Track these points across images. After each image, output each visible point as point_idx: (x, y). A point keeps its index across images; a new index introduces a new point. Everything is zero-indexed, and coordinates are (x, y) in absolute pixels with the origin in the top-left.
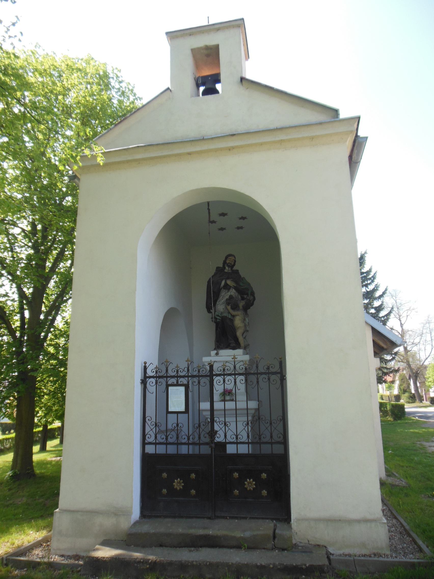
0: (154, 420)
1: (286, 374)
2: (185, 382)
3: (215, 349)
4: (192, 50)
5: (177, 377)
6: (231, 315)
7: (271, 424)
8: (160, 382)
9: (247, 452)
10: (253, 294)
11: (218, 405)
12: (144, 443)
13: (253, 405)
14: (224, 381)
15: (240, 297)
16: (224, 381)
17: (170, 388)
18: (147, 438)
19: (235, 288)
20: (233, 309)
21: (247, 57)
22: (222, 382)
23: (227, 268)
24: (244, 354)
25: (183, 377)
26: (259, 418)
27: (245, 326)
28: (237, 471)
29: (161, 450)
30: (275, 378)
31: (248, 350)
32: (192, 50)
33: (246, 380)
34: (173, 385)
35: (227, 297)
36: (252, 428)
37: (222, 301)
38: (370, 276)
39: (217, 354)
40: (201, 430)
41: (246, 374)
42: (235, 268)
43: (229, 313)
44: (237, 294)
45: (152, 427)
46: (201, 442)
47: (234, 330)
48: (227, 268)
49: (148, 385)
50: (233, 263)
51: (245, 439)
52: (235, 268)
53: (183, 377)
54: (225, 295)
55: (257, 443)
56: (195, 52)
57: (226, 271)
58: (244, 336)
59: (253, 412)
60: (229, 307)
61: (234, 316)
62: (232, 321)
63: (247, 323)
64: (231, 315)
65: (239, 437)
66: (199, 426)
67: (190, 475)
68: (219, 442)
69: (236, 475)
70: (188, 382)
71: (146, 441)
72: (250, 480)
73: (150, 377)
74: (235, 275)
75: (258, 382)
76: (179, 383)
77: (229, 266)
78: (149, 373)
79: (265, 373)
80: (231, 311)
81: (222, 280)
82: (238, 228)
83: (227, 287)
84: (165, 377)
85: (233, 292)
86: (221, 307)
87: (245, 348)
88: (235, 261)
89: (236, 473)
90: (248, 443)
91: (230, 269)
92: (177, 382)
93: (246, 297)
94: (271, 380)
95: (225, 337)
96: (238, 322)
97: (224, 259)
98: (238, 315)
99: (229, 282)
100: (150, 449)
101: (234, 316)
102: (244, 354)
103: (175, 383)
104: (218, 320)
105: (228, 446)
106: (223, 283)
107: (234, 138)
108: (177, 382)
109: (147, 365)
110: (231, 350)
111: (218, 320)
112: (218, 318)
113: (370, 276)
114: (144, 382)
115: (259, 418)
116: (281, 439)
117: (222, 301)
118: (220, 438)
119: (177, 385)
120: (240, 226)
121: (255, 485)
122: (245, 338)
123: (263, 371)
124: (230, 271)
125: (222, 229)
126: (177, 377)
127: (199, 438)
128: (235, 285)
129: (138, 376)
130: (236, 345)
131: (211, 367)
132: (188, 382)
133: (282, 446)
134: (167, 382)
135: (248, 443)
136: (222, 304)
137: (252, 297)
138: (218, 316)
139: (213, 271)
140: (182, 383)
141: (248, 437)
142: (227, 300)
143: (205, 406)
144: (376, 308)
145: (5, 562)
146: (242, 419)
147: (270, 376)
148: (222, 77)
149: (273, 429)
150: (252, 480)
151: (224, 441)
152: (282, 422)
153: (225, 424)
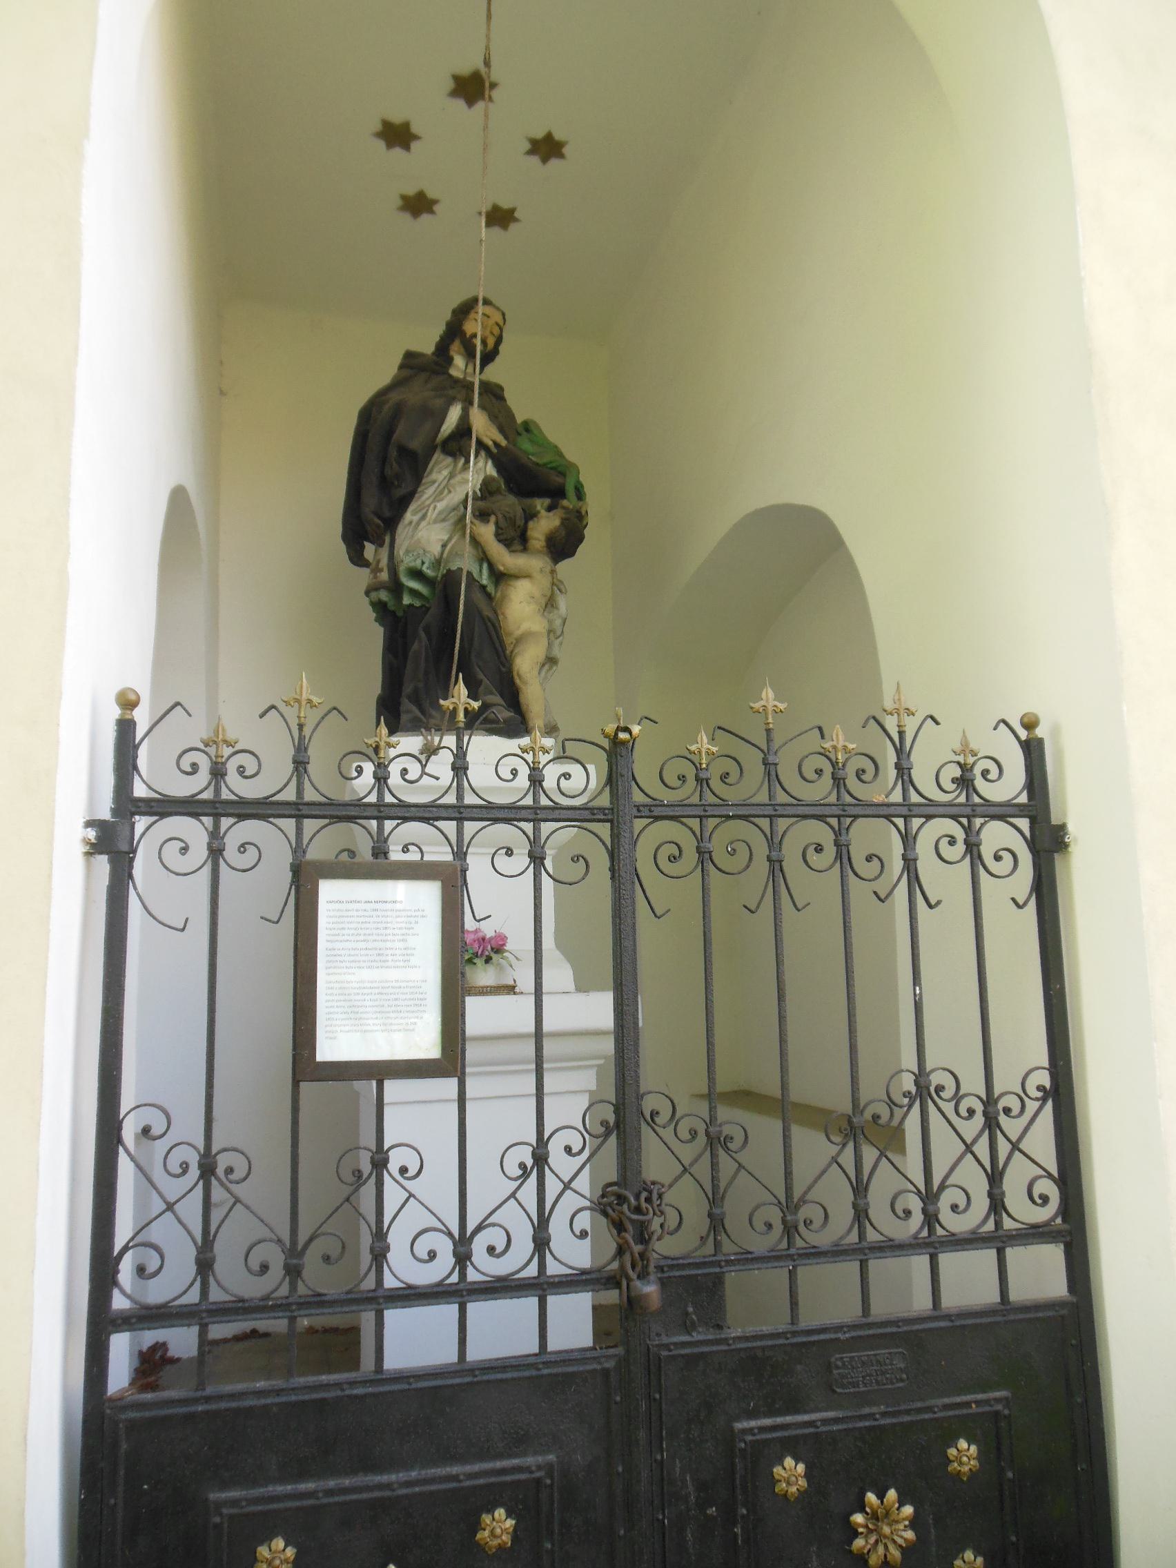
0: (190, 1127)
2: (440, 853)
7: (991, 1124)
8: (243, 848)
12: (101, 1323)
25: (428, 814)
28: (792, 1446)
34: (348, 868)
37: (440, 506)
40: (553, 1187)
43: (484, 557)
45: (173, 1188)
46: (553, 1268)
53: (428, 814)
60: (487, 532)
61: (499, 577)
66: (540, 1159)
67: (476, 1526)
69: (791, 1473)
71: (119, 1302)
72: (881, 1496)
73: (162, 807)
75: (910, 863)
80: (497, 551)
86: (430, 531)
89: (789, 1462)
96: (521, 608)
98: (528, 576)
104: (407, 600)
108: (380, 851)
111: (407, 600)
114: (111, 842)
119: (379, 866)
121: (914, 1523)
127: (541, 1243)
129: (77, 790)
132: (460, 854)
133: (1052, 1256)
134: (298, 849)
136: (435, 522)
139: (385, 372)
140: (413, 856)
149: (1003, 1148)
150: (892, 1494)
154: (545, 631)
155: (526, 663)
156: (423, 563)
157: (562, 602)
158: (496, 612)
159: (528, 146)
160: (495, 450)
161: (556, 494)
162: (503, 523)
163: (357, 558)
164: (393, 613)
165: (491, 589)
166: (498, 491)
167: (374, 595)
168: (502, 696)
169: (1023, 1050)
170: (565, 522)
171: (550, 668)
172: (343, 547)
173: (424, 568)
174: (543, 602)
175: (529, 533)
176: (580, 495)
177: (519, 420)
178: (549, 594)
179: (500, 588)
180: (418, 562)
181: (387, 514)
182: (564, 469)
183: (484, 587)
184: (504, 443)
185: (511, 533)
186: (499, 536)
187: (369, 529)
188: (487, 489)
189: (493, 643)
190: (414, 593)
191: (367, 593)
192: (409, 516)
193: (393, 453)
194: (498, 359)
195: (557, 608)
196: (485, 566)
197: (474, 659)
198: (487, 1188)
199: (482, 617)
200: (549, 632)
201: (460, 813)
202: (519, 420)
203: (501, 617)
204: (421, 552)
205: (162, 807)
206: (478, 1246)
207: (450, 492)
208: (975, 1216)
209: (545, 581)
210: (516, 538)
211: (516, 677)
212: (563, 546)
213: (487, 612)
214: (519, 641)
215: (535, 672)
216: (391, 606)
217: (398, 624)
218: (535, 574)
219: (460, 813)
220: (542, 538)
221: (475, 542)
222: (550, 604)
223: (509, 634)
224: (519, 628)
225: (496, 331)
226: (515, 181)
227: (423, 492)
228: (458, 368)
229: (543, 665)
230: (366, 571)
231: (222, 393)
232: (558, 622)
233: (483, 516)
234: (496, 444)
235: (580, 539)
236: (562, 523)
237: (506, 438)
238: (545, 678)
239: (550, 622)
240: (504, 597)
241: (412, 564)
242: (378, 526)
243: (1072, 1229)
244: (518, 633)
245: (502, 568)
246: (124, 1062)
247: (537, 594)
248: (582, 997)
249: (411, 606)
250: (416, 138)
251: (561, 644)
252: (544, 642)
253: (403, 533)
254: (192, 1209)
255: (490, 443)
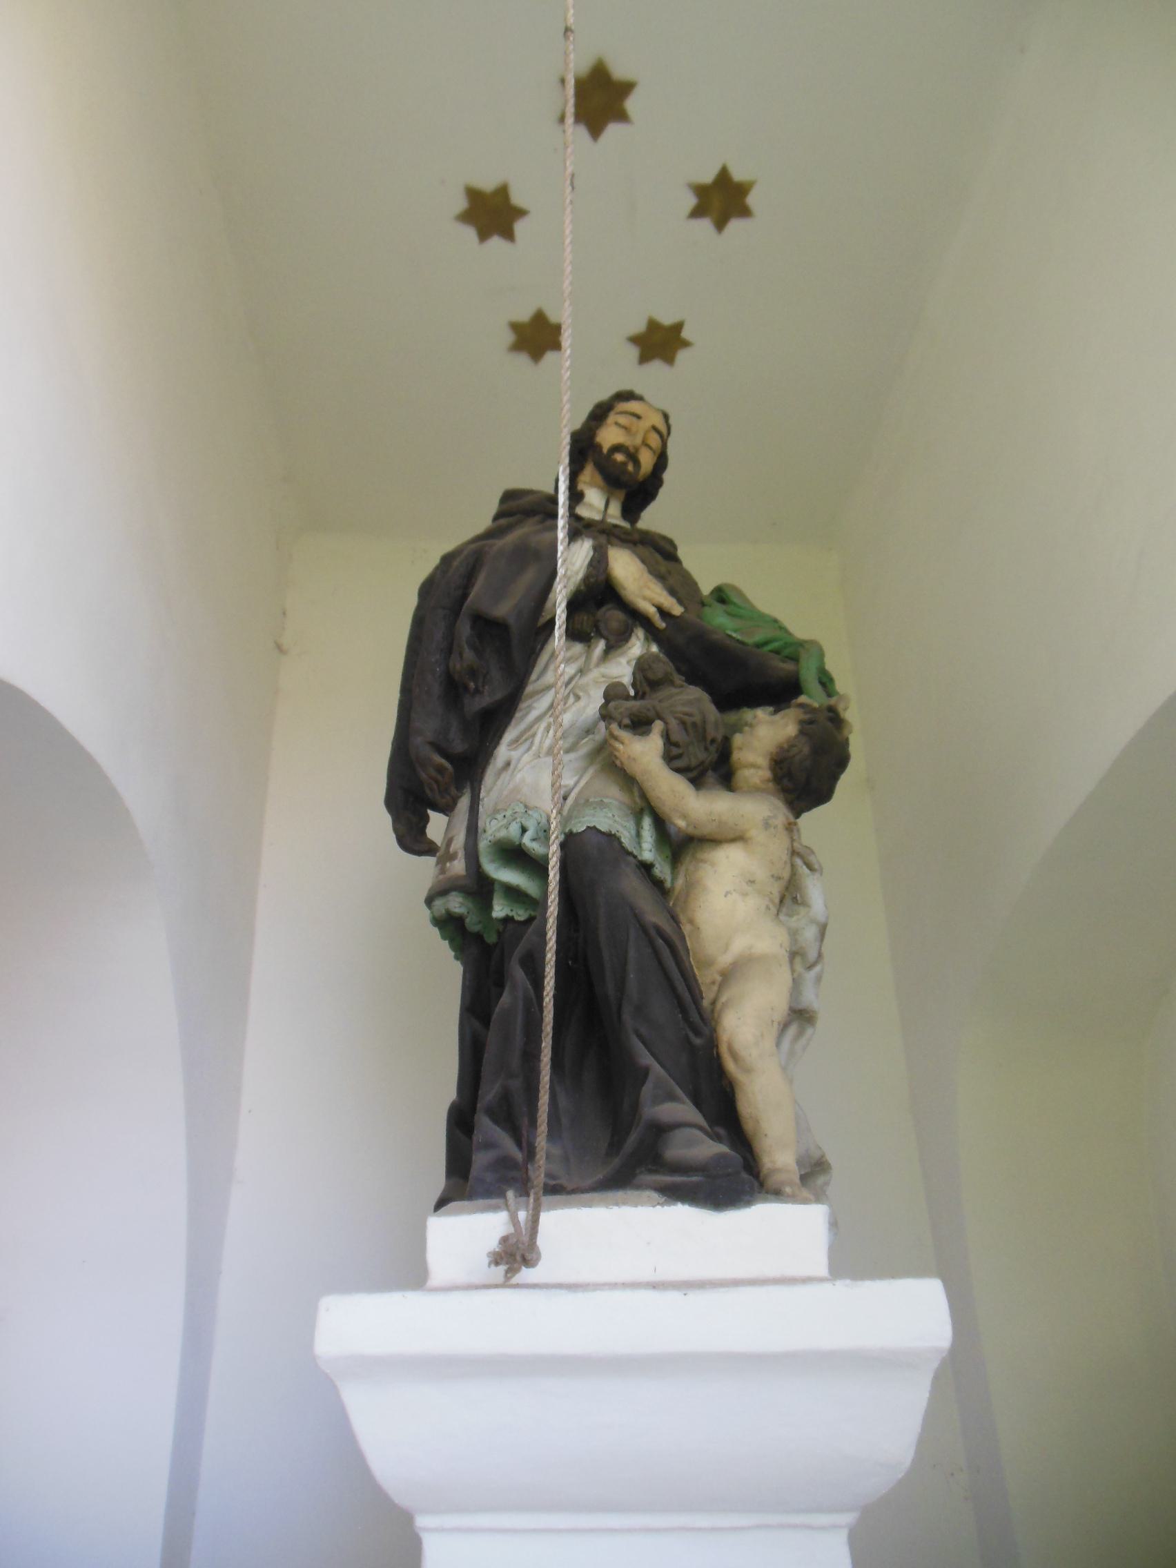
6: (660, 824)
24: (853, 1258)
39: (515, 1255)
43: (645, 807)
50: (647, 460)
60: (645, 753)
61: (682, 845)
64: (660, 824)
80: (670, 788)
86: (538, 778)
96: (727, 907)
101: (682, 845)
102: (853, 1258)
104: (500, 909)
110: (683, 1213)
111: (500, 909)
145: (764, 734)
154: (783, 955)
155: (746, 1024)
156: (524, 830)
157: (814, 890)
158: (674, 919)
159: (691, 201)
160: (661, 624)
161: (780, 692)
162: (678, 735)
163: (412, 837)
164: (479, 937)
165: (662, 870)
166: (664, 681)
167: (439, 903)
168: (697, 1103)
170: (806, 728)
171: (800, 1034)
172: (386, 819)
173: (526, 840)
174: (776, 889)
175: (736, 756)
176: (826, 682)
177: (706, 588)
178: (786, 874)
179: (682, 870)
180: (514, 830)
181: (459, 746)
182: (794, 650)
183: (646, 867)
184: (677, 610)
185: (698, 755)
186: (671, 757)
187: (423, 776)
188: (646, 679)
189: (673, 989)
190: (513, 893)
191: (429, 901)
192: (503, 752)
193: (465, 629)
194: (663, 493)
195: (805, 904)
196: (647, 822)
197: (627, 1016)
199: (643, 928)
200: (795, 954)
202: (706, 588)
203: (686, 929)
204: (520, 809)
207: (578, 698)
209: (778, 847)
210: (713, 767)
211: (724, 1049)
212: (807, 779)
213: (653, 916)
214: (727, 976)
215: (769, 1043)
216: (472, 924)
217: (486, 954)
218: (753, 833)
220: (763, 761)
221: (628, 780)
222: (789, 896)
223: (708, 963)
224: (726, 948)
225: (654, 440)
226: (684, 270)
227: (530, 708)
228: (591, 506)
229: (785, 1027)
230: (429, 862)
231: (279, 648)
232: (810, 933)
233: (640, 725)
234: (663, 613)
235: (842, 762)
236: (802, 732)
237: (680, 602)
238: (792, 1053)
239: (794, 934)
240: (690, 886)
241: (502, 834)
242: (440, 770)
244: (725, 960)
245: (681, 823)
247: (761, 874)
248: (844, 1290)
249: (507, 920)
250: (520, 213)
251: (819, 979)
252: (783, 977)
253: (494, 788)
255: (651, 610)
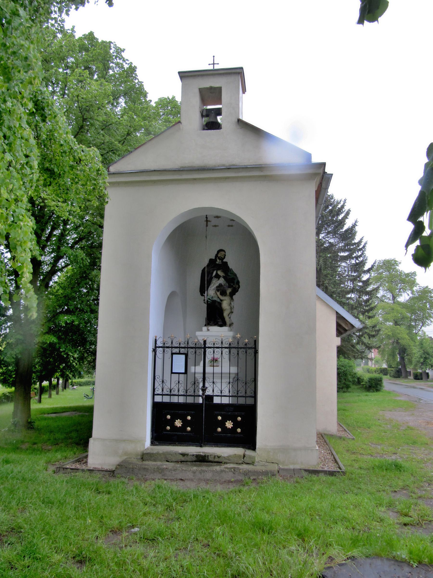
1: (258, 349)
3: (205, 325)
4: (200, 89)
5: (180, 348)
7: (246, 383)
9: (228, 403)
10: (238, 282)
11: (209, 369)
12: (154, 395)
13: (234, 370)
14: (214, 352)
15: (227, 284)
16: (214, 352)
17: (174, 356)
18: (156, 390)
19: (224, 277)
20: (221, 294)
21: (244, 91)
22: (212, 352)
23: (218, 260)
26: (238, 379)
27: (231, 308)
29: (166, 399)
30: (252, 351)
31: (232, 327)
32: (200, 89)
33: (230, 352)
35: (217, 285)
36: (232, 386)
38: (361, 247)
40: (196, 386)
41: (230, 348)
42: (224, 260)
43: (218, 297)
44: (225, 282)
47: (221, 311)
48: (218, 260)
49: (157, 353)
50: (223, 257)
51: (227, 393)
52: (224, 260)
54: (215, 283)
55: (235, 396)
56: (201, 91)
57: (217, 263)
58: (229, 316)
59: (234, 376)
60: (218, 293)
61: (221, 300)
62: (220, 304)
63: (232, 307)
65: (223, 392)
68: (209, 395)
70: (188, 352)
73: (159, 347)
74: (225, 267)
76: (181, 352)
77: (220, 259)
78: (159, 344)
79: (243, 348)
81: (214, 271)
82: (229, 226)
83: (218, 276)
84: (170, 347)
85: (222, 281)
86: (212, 292)
87: (230, 325)
88: (225, 255)
90: (229, 396)
91: (220, 261)
92: (180, 351)
93: (232, 284)
94: (248, 353)
95: (215, 316)
96: (225, 305)
97: (216, 253)
99: (220, 273)
100: (158, 399)
103: (178, 352)
105: (214, 397)
106: (215, 273)
107: (230, 170)
109: (157, 338)
110: (219, 327)
112: (209, 300)
113: (361, 247)
114: (155, 351)
115: (238, 379)
116: (253, 394)
117: (213, 287)
118: (209, 392)
120: (231, 224)
122: (230, 318)
123: (243, 346)
124: (221, 263)
125: (215, 226)
126: (180, 348)
128: (224, 275)
129: (151, 346)
130: (223, 324)
131: (205, 342)
133: (253, 399)
134: (172, 351)
135: (229, 396)
137: (237, 286)
138: (209, 299)
141: (229, 392)
142: (217, 287)
143: (199, 369)
144: (363, 282)
146: (226, 380)
147: (247, 351)
148: (223, 113)
151: (212, 394)
152: (254, 383)
153: (213, 382)
155: (225, 314)
169: (250, 376)
198: (189, 386)
201: (188, 348)
205: (159, 347)
206: (188, 391)
208: (243, 394)
219: (188, 348)
243: (255, 397)
246: (257, 431)
254: (161, 385)
